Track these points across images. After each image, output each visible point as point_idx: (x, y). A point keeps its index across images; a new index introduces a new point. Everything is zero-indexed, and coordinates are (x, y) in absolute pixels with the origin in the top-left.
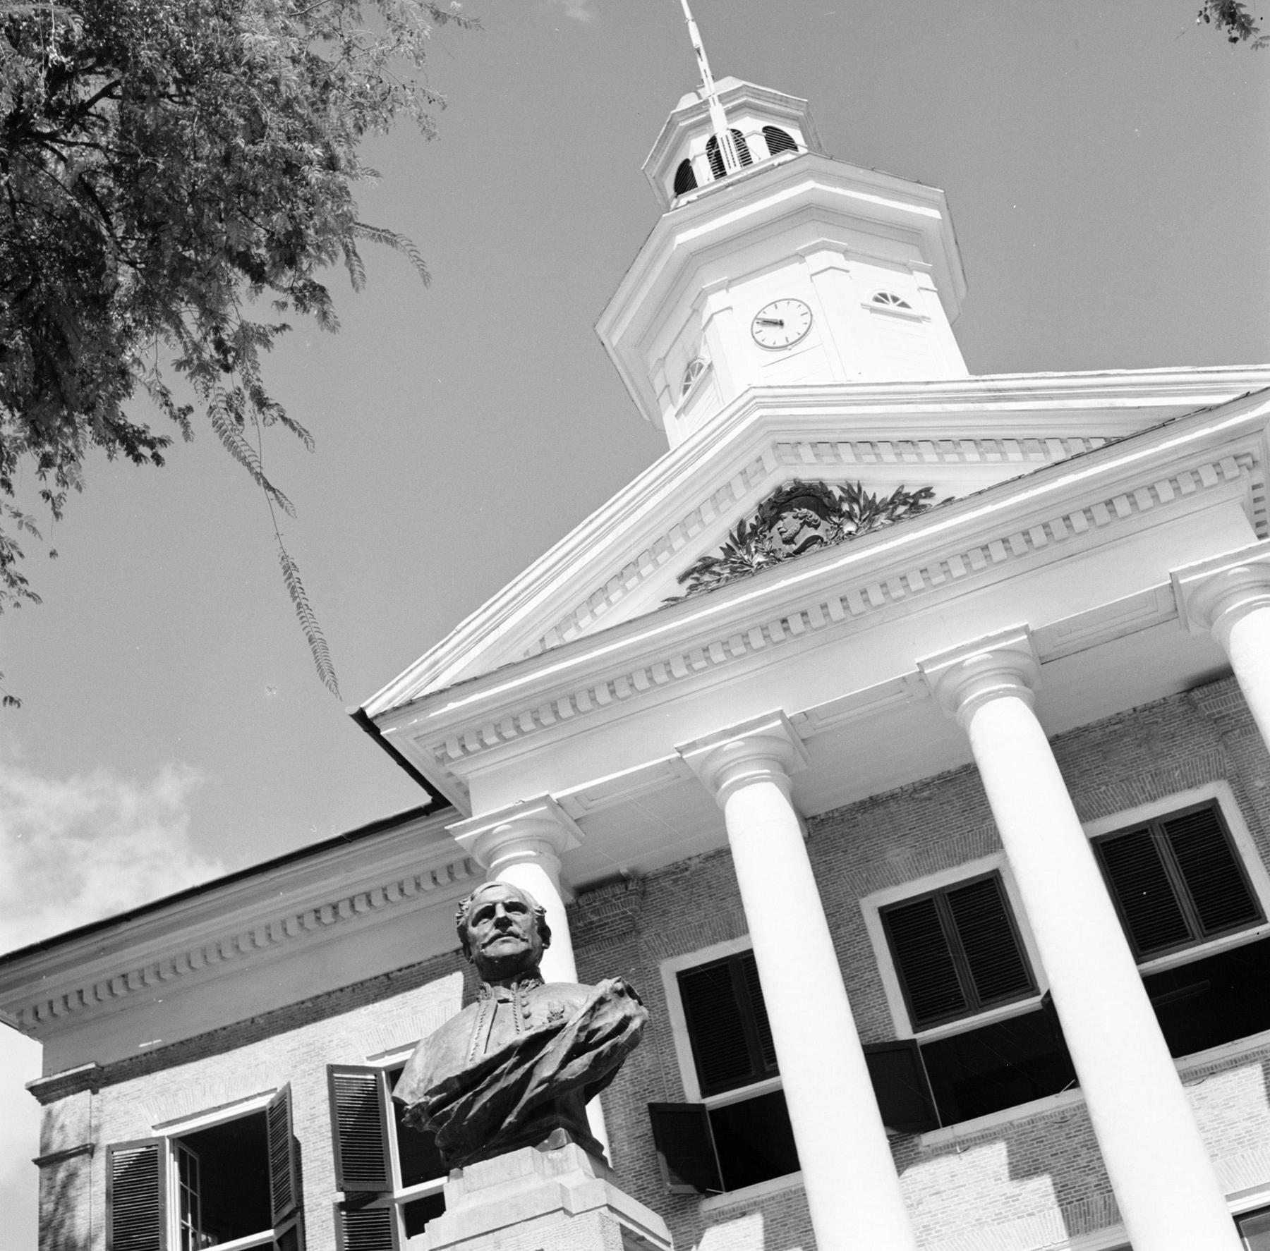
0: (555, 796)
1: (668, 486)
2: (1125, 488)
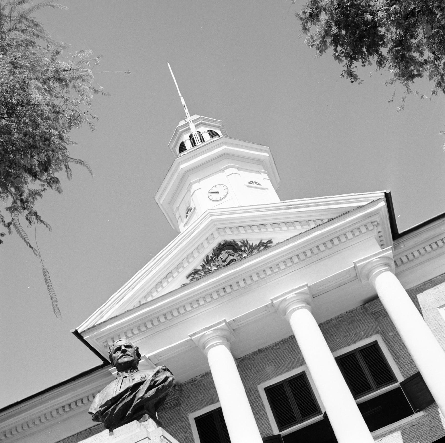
1: (181, 245)
2: (336, 235)
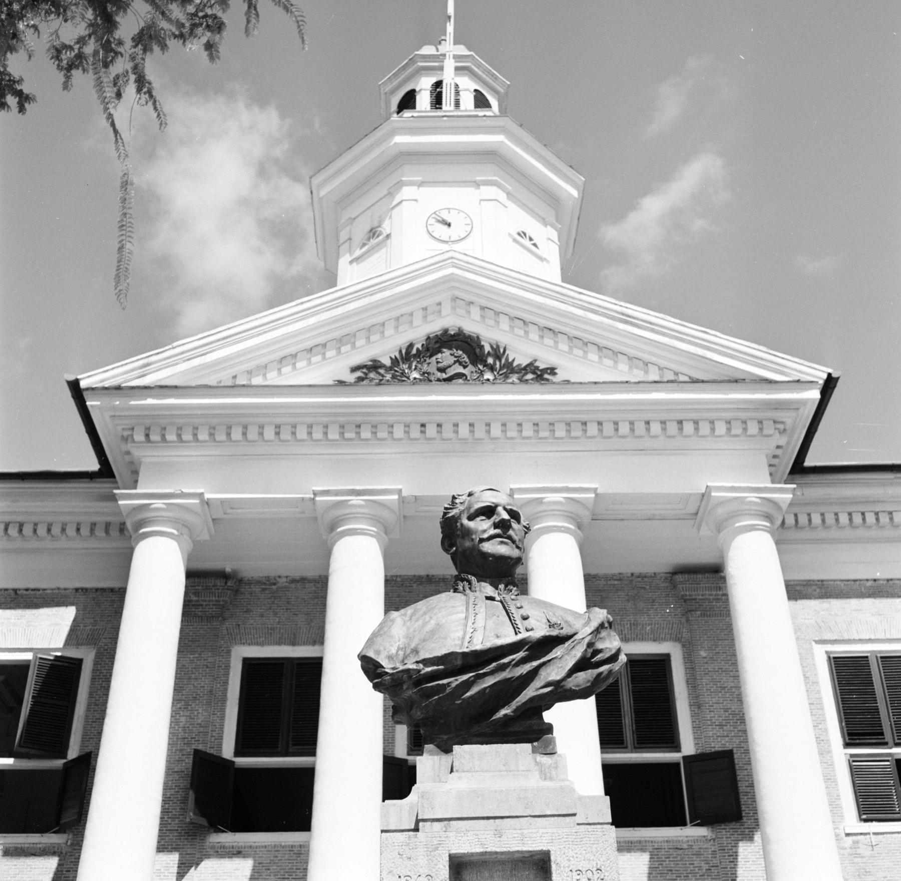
0: (207, 496)
2: (694, 416)
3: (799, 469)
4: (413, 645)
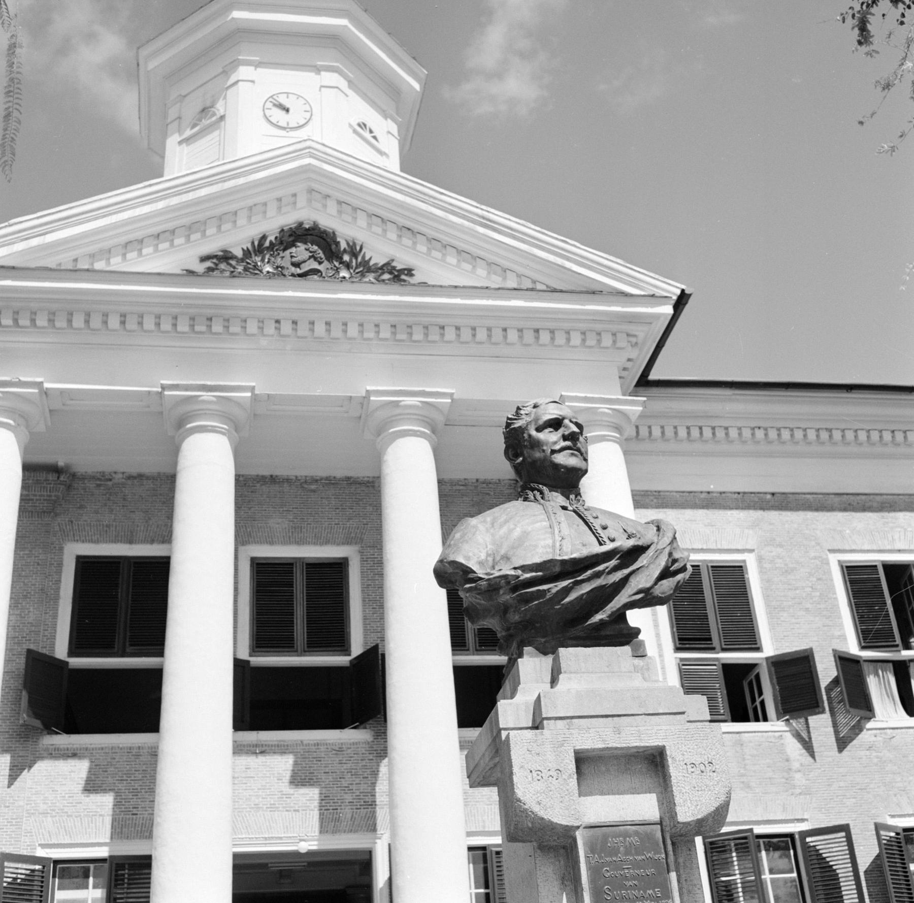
0: (47, 385)
1: (220, 185)
2: (551, 325)
3: (644, 382)
4: (503, 552)
